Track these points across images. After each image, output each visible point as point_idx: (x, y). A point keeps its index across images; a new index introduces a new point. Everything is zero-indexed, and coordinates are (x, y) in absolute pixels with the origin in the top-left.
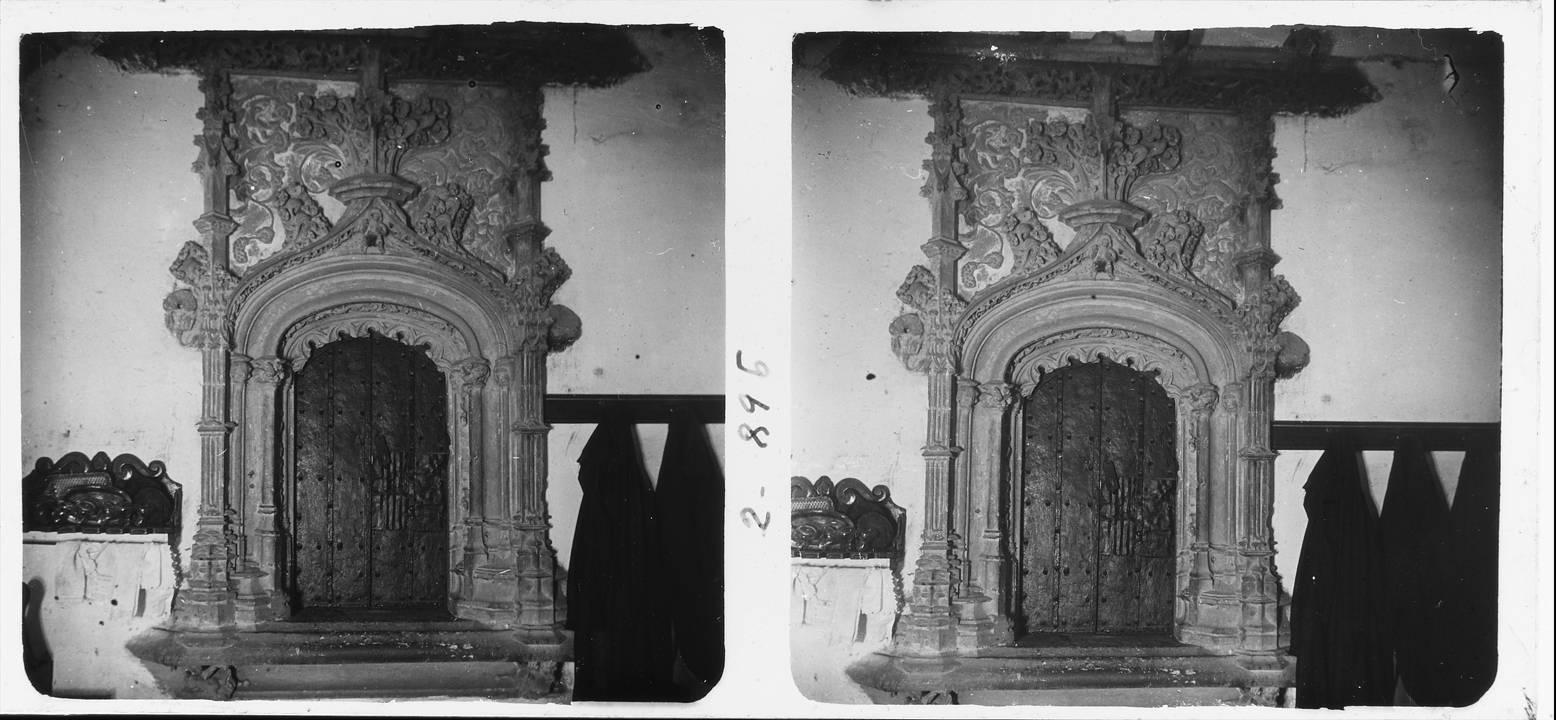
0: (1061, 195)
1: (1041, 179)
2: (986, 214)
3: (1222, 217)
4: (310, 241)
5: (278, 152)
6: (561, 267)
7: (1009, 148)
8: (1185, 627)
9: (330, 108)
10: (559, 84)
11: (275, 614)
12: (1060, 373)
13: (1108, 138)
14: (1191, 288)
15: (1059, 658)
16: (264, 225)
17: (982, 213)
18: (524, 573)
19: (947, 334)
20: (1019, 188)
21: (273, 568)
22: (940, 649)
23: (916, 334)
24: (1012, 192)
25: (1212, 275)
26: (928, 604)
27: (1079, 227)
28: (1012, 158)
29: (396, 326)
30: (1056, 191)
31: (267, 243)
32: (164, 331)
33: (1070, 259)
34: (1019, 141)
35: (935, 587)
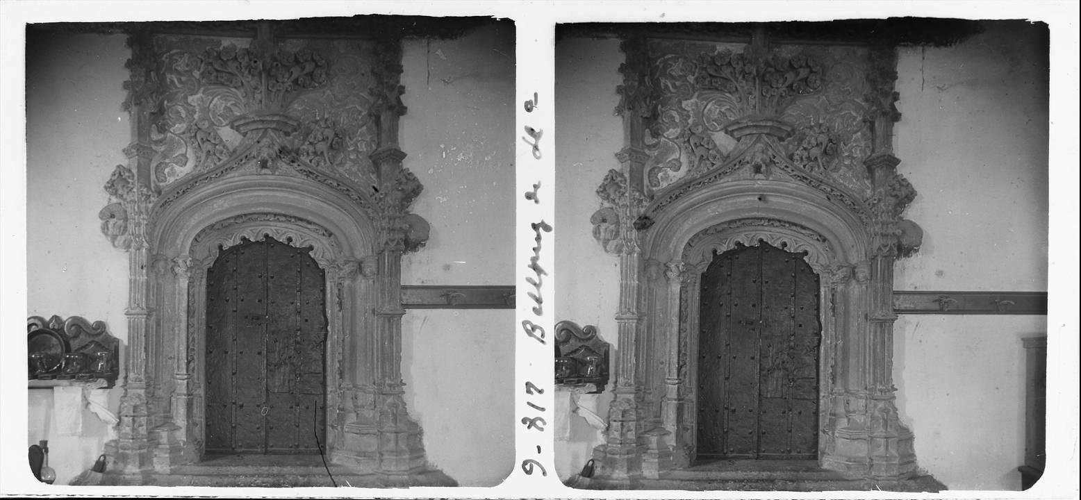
0: (233, 108)
1: (711, 101)
2: (668, 129)
3: (855, 129)
4: (708, 169)
5: (192, 95)
6: (910, 189)
7: (685, 76)
8: (825, 455)
9: (732, 62)
10: (910, 44)
11: (186, 460)
12: (234, 249)
13: (762, 65)
14: (337, 180)
15: (234, 475)
16: (673, 157)
17: (665, 128)
18: (875, 434)
19: (144, 219)
20: (694, 107)
21: (186, 423)
22: (140, 467)
23: (612, 224)
24: (194, 106)
25: (353, 169)
26: (130, 432)
27: (740, 138)
28: (688, 84)
29: (285, 233)
30: (723, 110)
31: (675, 171)
32: (592, 240)
33: (240, 158)
34: (693, 70)
35: (136, 418)
